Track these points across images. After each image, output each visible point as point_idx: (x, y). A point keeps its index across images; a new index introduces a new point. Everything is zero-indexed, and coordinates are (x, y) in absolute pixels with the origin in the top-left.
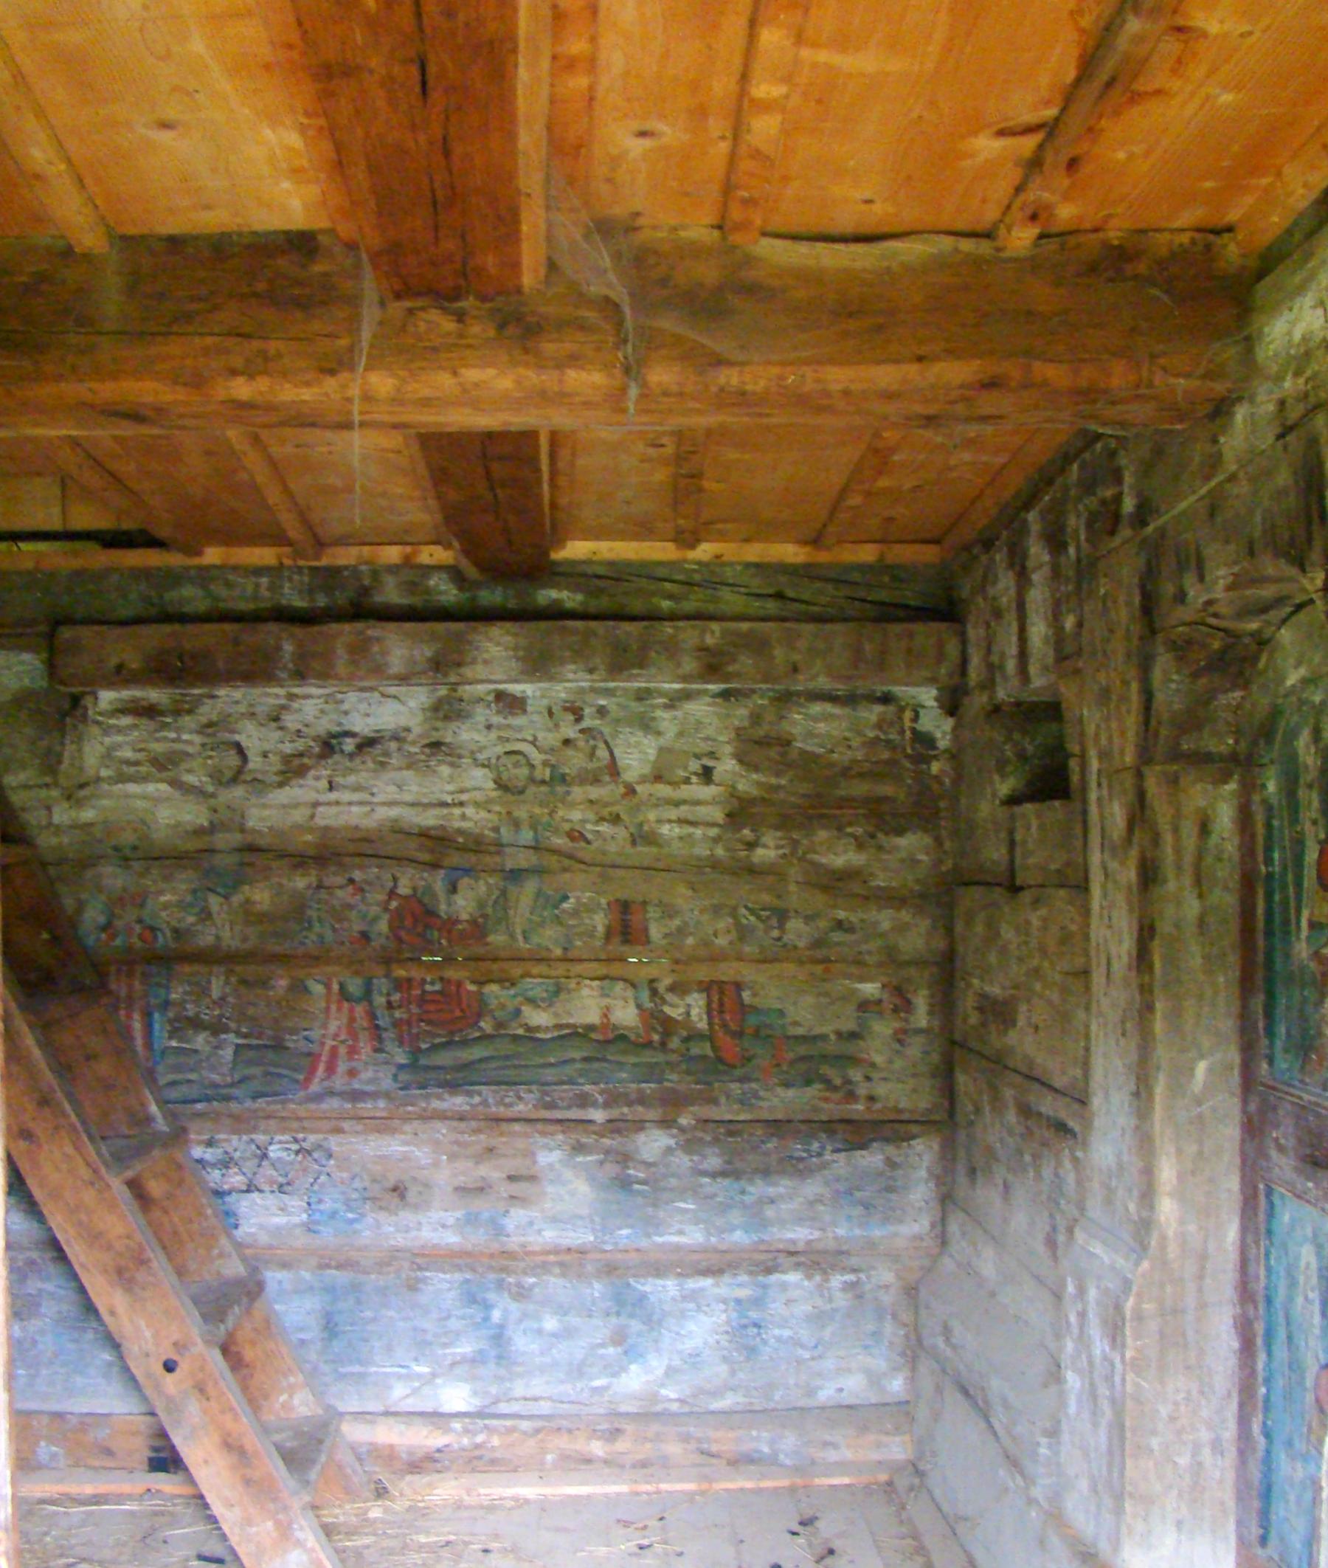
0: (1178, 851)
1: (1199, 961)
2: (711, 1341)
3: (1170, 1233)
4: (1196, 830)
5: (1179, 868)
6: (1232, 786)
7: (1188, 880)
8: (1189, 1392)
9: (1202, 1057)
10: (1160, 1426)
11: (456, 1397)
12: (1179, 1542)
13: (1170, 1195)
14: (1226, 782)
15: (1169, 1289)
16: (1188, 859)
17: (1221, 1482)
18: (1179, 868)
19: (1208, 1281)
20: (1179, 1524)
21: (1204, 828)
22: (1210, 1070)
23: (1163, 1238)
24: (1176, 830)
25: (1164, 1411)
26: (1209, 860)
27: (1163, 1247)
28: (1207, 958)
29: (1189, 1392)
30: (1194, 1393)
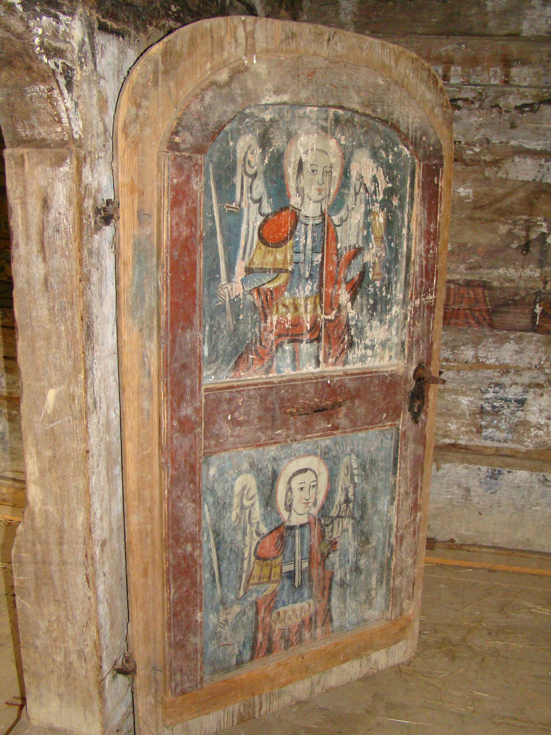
0: (26, 222)
1: (45, 312)
2: (379, 494)
3: (37, 509)
4: (39, 204)
5: (28, 237)
6: (64, 169)
7: (35, 248)
8: (59, 617)
9: (51, 386)
10: (41, 633)
11: (402, 490)
12: (62, 706)
13: (34, 483)
14: (60, 165)
15: (39, 547)
16: (34, 230)
17: (86, 677)
18: (28, 237)
19: (65, 547)
20: (60, 696)
21: (46, 204)
22: (58, 397)
23: (33, 512)
24: (24, 204)
25: (43, 625)
26: (49, 232)
27: (33, 519)
28: (51, 310)
29: (59, 617)
30: (63, 618)
